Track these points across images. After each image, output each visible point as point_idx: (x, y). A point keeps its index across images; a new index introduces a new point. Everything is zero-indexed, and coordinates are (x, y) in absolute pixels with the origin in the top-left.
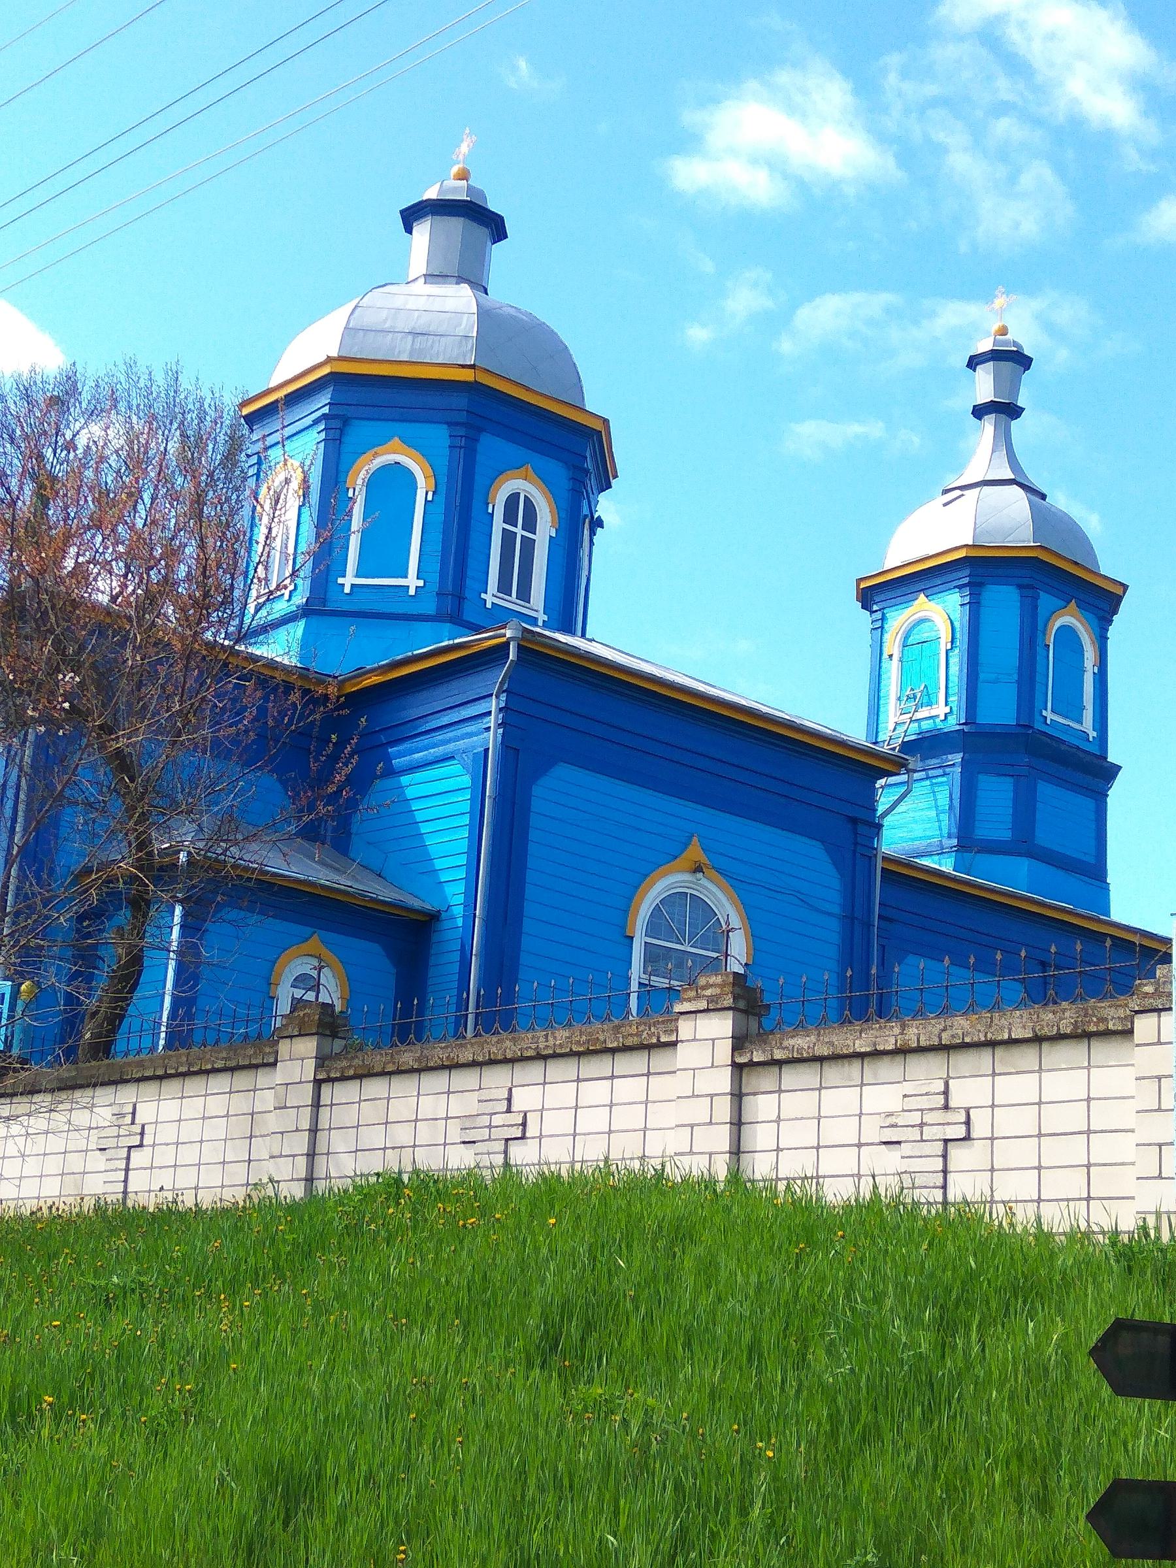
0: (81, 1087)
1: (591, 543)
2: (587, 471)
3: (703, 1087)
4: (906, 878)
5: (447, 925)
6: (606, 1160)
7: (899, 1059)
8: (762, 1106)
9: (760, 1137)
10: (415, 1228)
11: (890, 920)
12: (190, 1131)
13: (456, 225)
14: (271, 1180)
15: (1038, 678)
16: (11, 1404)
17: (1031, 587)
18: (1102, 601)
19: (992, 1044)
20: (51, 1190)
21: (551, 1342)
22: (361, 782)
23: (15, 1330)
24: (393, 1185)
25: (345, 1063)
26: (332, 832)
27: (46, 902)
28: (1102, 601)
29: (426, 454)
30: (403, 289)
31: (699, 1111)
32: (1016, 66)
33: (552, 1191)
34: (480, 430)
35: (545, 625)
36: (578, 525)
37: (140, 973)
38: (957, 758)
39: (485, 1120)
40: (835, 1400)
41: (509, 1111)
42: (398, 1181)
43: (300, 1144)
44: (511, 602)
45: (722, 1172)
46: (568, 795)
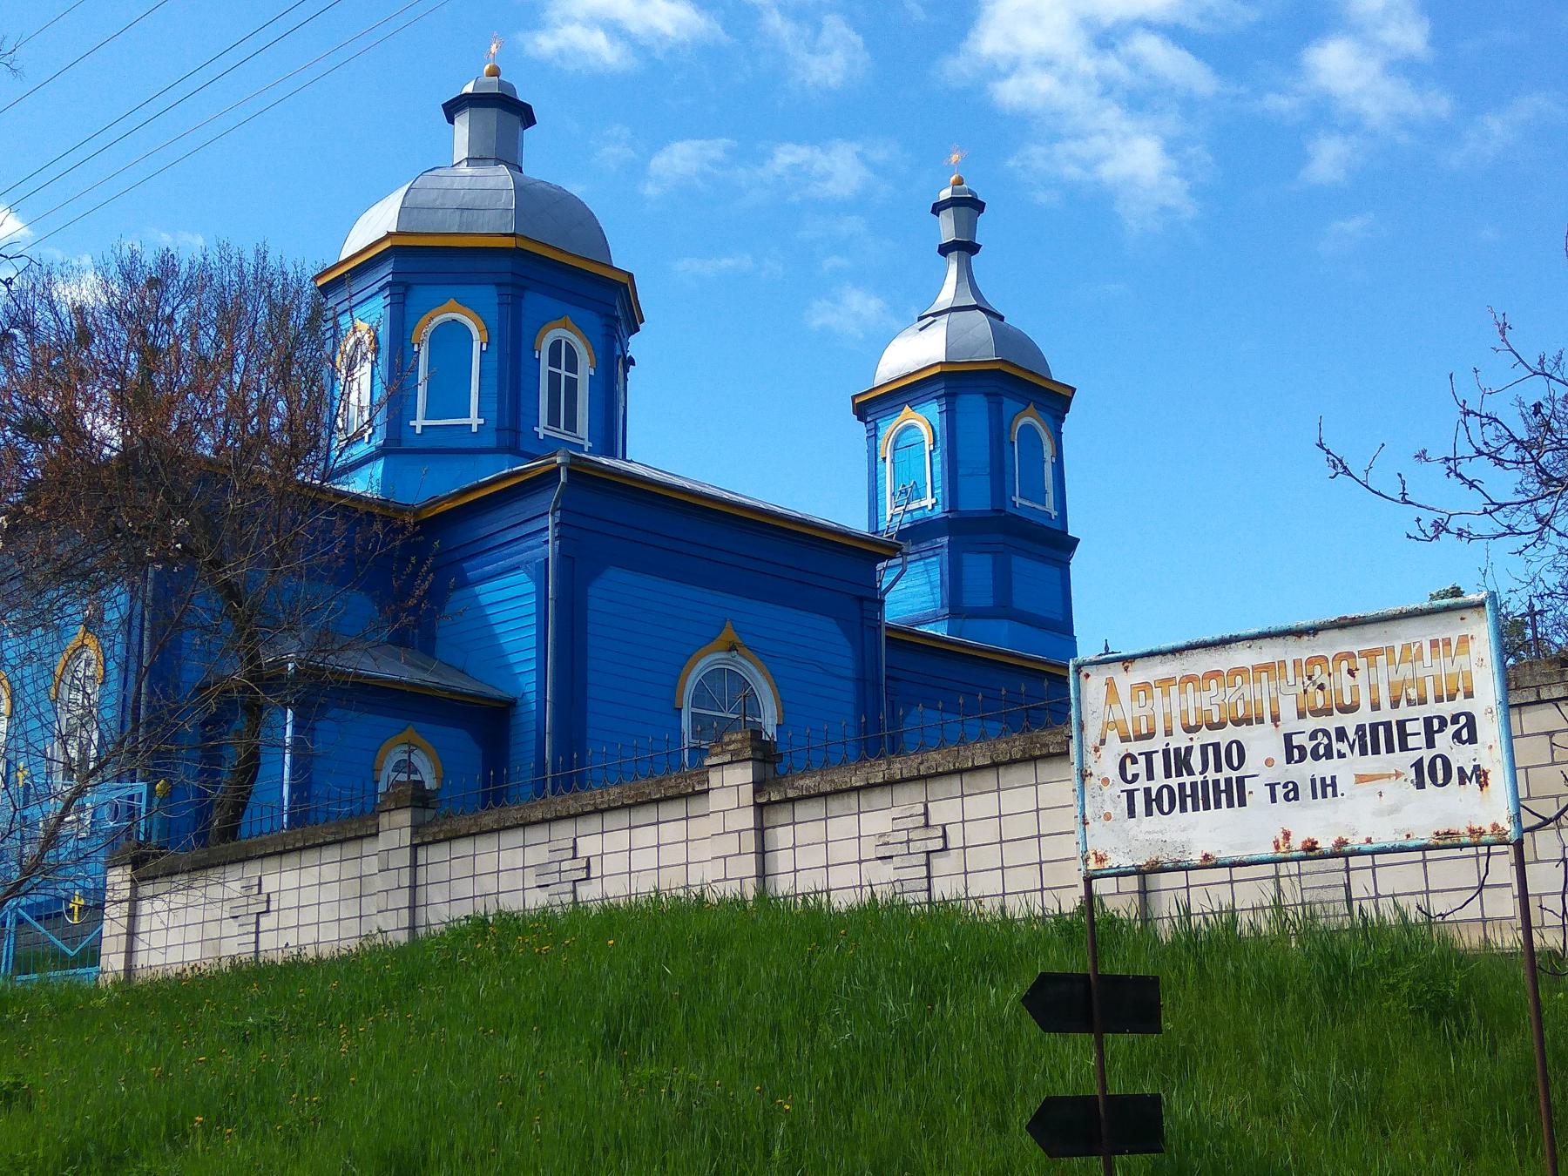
0: (213, 866)
1: (626, 379)
2: (617, 319)
3: (731, 826)
4: (906, 642)
5: (522, 710)
6: (657, 891)
7: (887, 789)
8: (781, 836)
9: (782, 862)
10: (499, 957)
11: (897, 680)
12: (310, 896)
13: (491, 115)
14: (380, 931)
15: (1008, 469)
16: (168, 1126)
17: (996, 394)
18: (1056, 401)
19: (960, 772)
20: (193, 954)
21: (612, 1039)
22: (438, 596)
23: (168, 1068)
24: (480, 924)
25: (436, 829)
26: (417, 635)
27: (172, 712)
28: (1056, 401)
29: (478, 313)
30: (451, 172)
31: (730, 845)
33: (613, 918)
34: (524, 288)
35: (591, 451)
36: (613, 367)
37: (257, 767)
38: (945, 540)
39: (555, 867)
40: (838, 1061)
41: (574, 857)
42: (484, 921)
43: (403, 898)
44: (560, 433)
45: (750, 893)
46: (617, 593)
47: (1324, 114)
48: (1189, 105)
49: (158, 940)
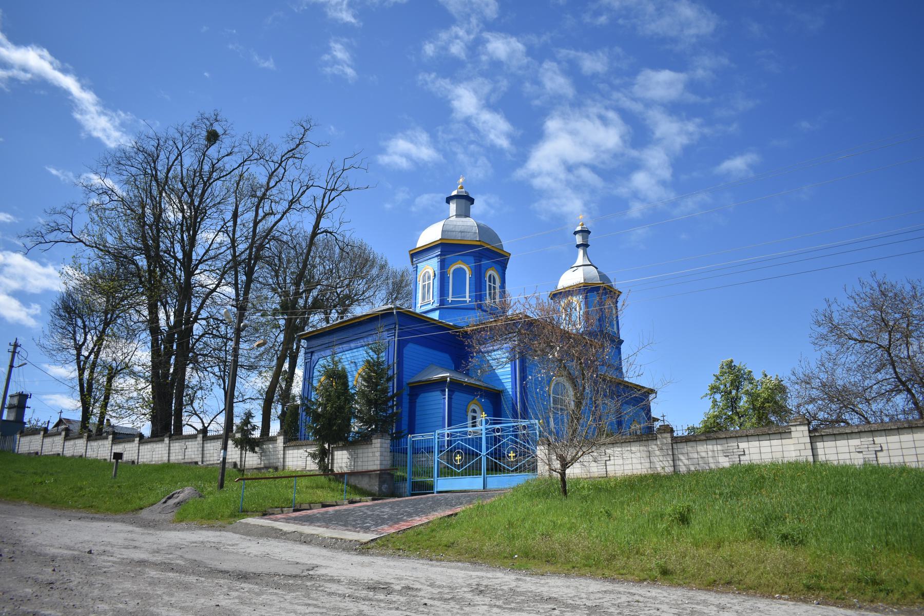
8: (819, 445)
9: (820, 451)
32: (475, 130)
47: (636, 195)
48: (593, 191)
49: (291, 459)
